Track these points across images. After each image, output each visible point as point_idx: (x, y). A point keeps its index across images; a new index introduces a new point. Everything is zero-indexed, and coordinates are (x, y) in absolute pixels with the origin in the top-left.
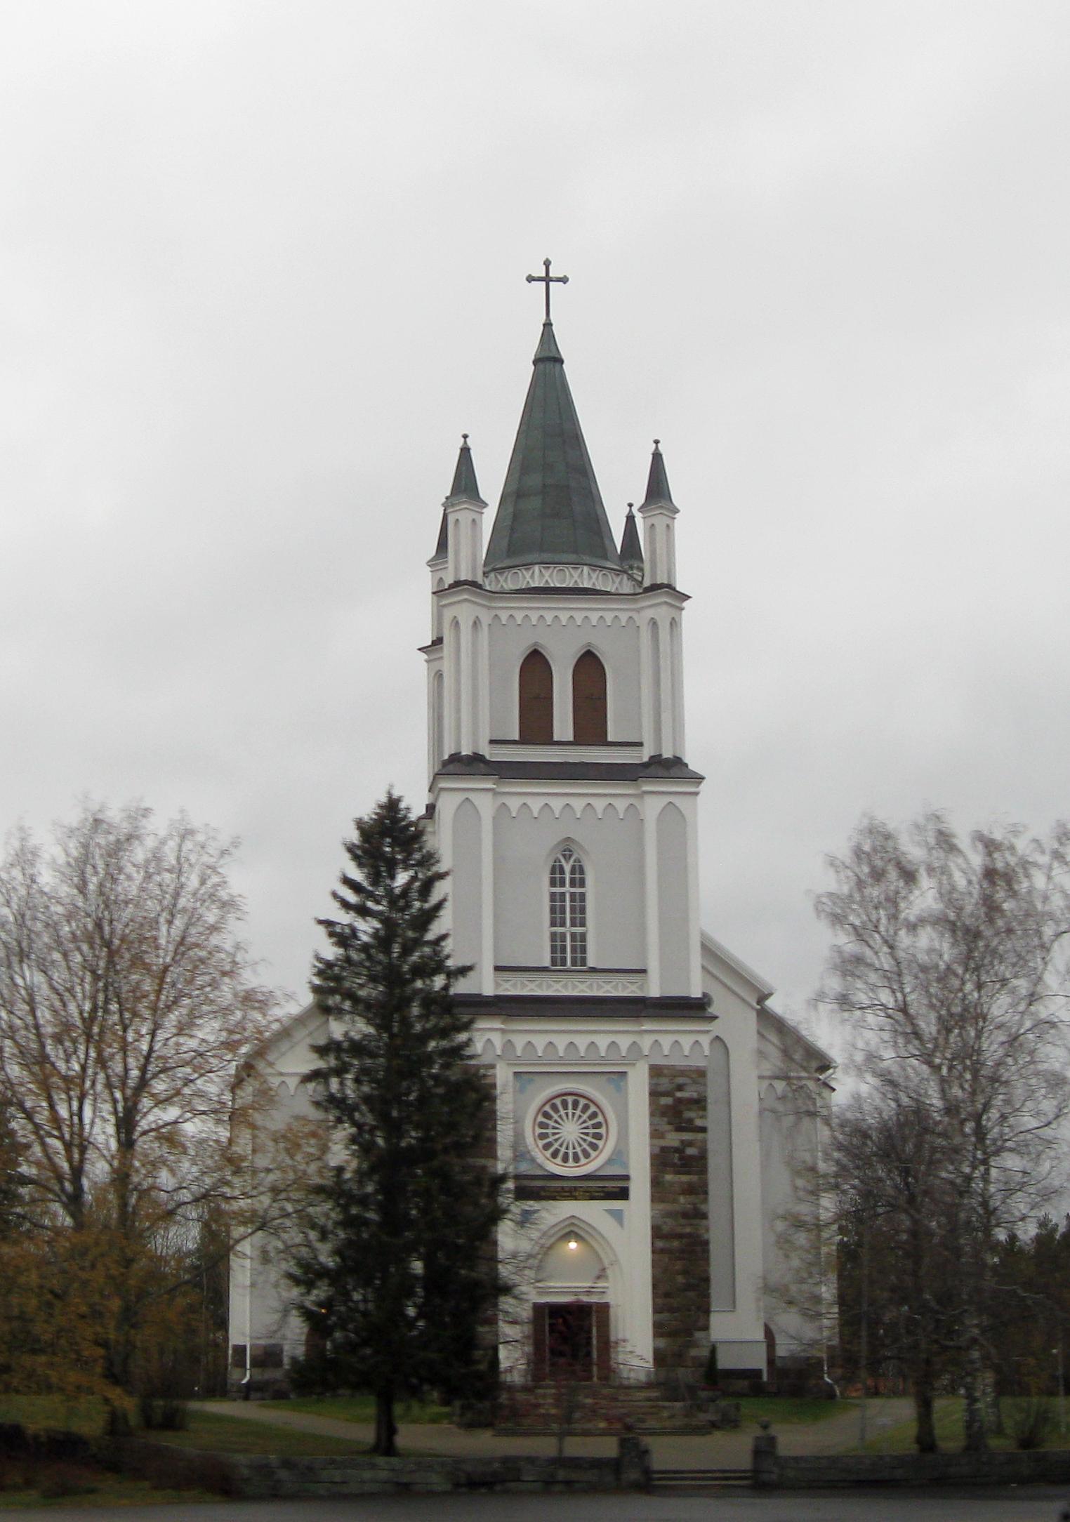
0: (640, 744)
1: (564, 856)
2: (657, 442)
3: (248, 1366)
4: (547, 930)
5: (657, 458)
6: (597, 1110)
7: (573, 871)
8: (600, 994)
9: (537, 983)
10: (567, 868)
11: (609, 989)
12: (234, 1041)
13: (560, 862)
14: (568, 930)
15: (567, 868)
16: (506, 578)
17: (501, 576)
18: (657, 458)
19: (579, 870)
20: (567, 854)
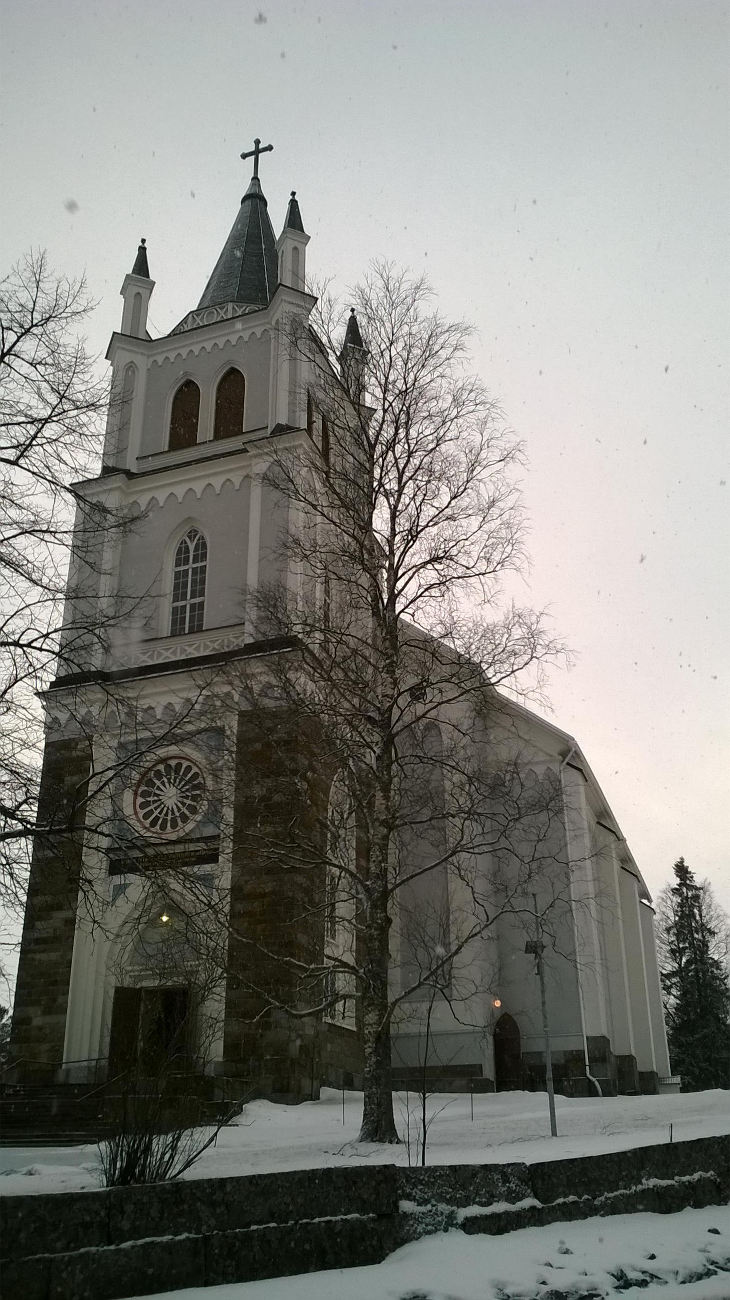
0: (267, 427)
1: (190, 538)
2: (293, 194)
3: (587, 1063)
4: (206, 599)
5: (142, 250)
6: (190, 764)
7: (196, 548)
8: (160, 661)
9: (195, 646)
10: (192, 547)
11: (146, 659)
12: (189, 733)
13: (186, 542)
14: (189, 602)
15: (192, 547)
16: (203, 317)
17: (221, 309)
18: (142, 250)
19: (202, 545)
20: (192, 534)
